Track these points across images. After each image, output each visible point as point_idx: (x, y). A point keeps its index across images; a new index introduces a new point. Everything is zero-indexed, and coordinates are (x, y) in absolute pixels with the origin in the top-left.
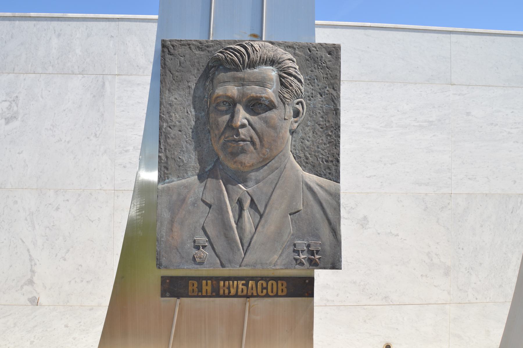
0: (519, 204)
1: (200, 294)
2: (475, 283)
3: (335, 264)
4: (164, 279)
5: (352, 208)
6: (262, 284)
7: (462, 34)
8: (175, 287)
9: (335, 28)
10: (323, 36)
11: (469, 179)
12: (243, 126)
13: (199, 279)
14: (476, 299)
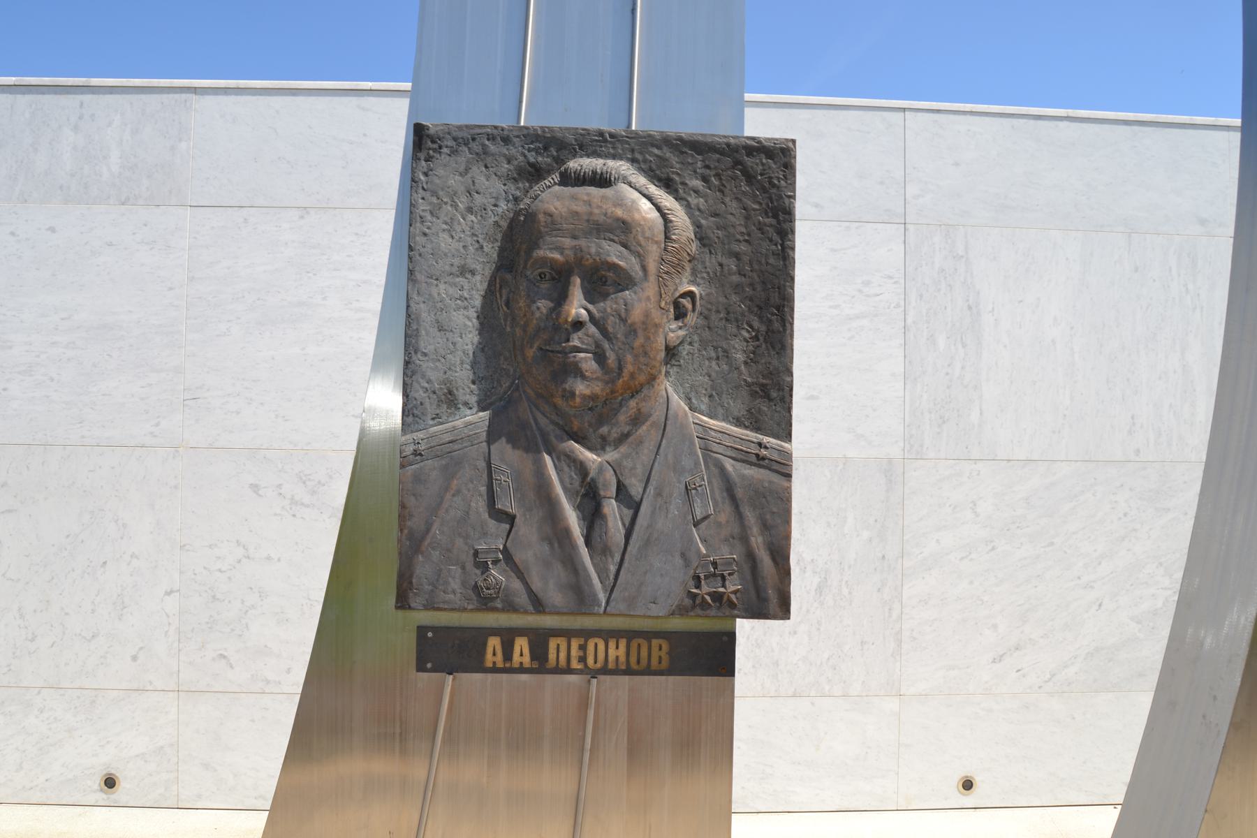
1: (508, 665)
3: (772, 601)
4: (421, 630)
5: (319, 482)
8: (448, 652)
9: (294, 95)
10: (760, 124)
12: (578, 325)
13: (508, 637)
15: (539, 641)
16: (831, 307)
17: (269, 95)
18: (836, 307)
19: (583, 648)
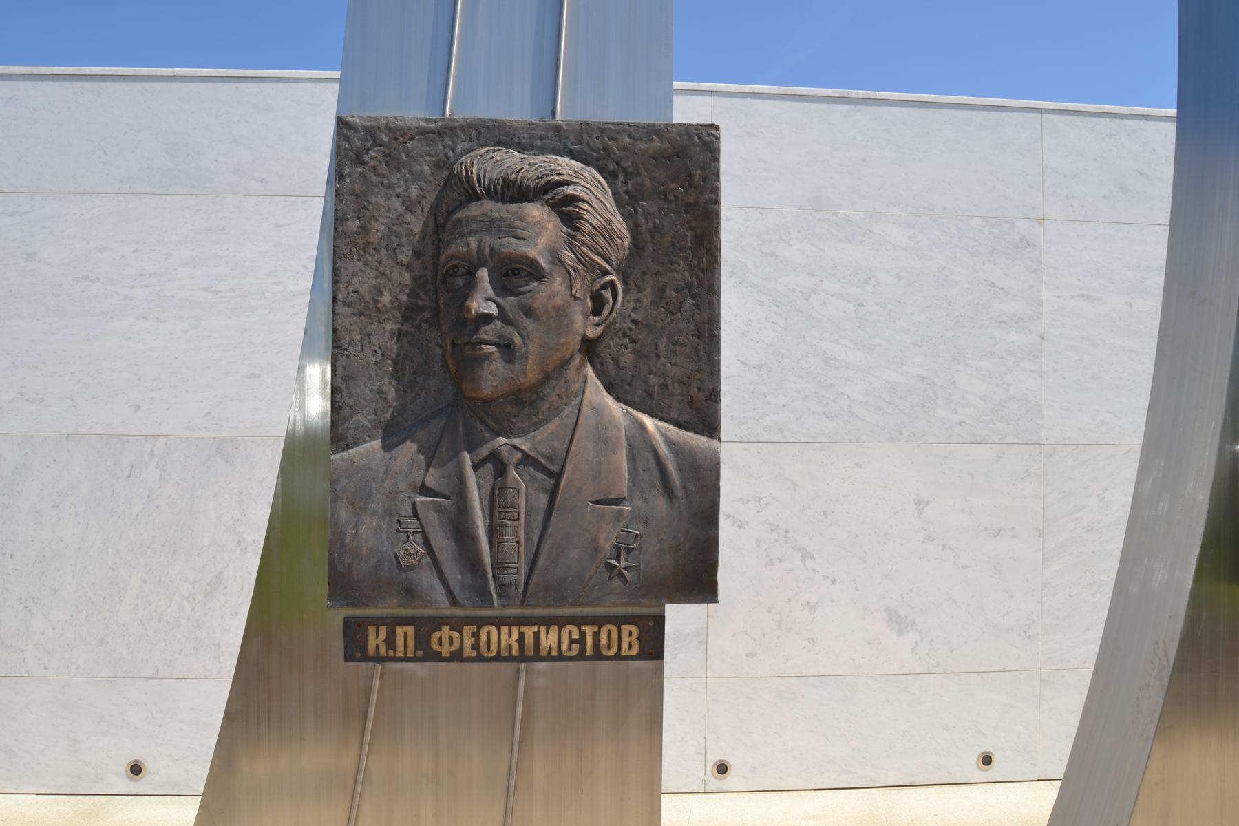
0: (146, 459)
1: (391, 653)
2: (42, 633)
3: (699, 582)
6: (570, 632)
7: (24, 80)
10: (687, 110)
11: (28, 400)
12: (486, 318)
13: (392, 623)
14: (46, 668)
15: (425, 627)
16: (274, 283)
17: (813, 102)
18: (281, 283)
19: (476, 635)
